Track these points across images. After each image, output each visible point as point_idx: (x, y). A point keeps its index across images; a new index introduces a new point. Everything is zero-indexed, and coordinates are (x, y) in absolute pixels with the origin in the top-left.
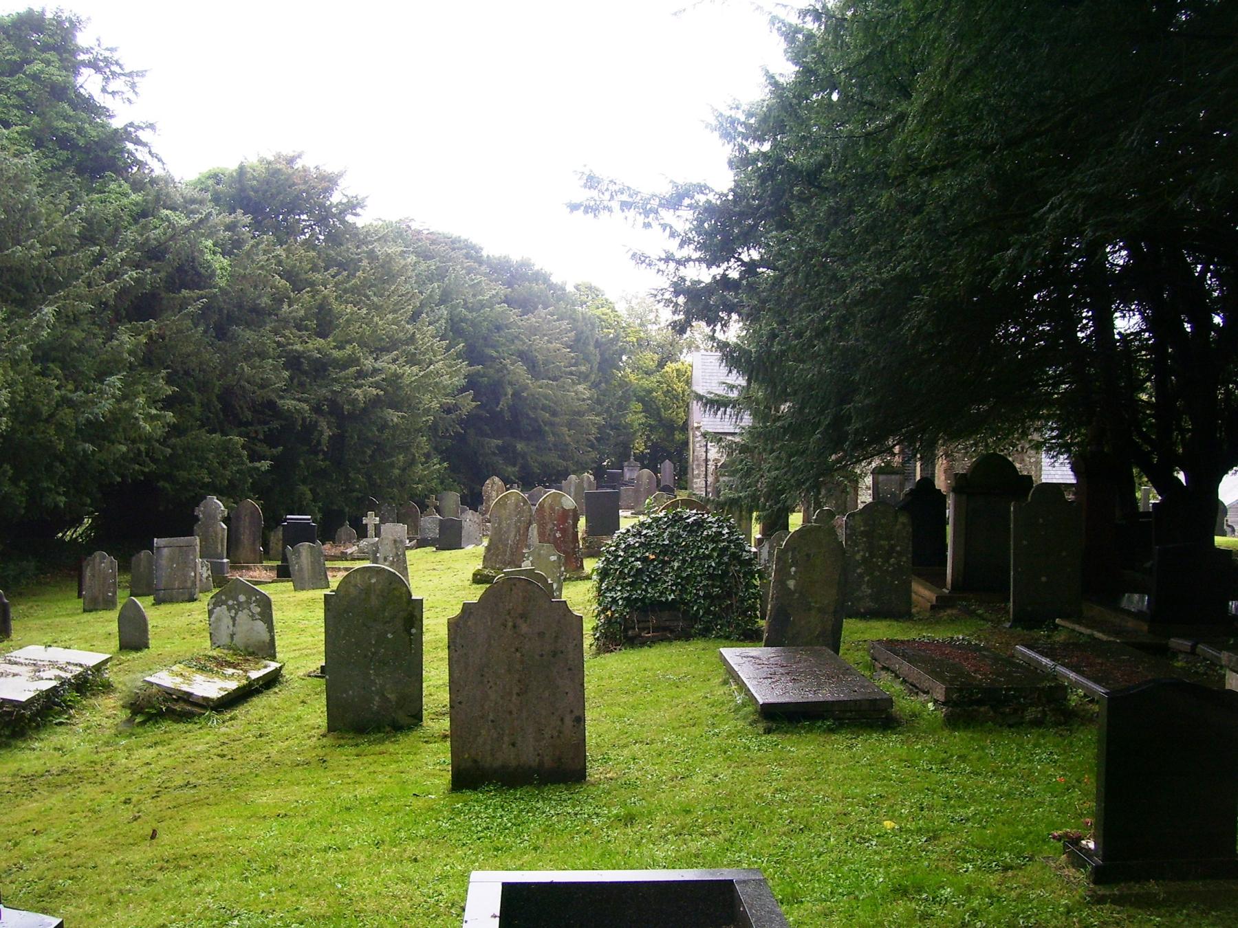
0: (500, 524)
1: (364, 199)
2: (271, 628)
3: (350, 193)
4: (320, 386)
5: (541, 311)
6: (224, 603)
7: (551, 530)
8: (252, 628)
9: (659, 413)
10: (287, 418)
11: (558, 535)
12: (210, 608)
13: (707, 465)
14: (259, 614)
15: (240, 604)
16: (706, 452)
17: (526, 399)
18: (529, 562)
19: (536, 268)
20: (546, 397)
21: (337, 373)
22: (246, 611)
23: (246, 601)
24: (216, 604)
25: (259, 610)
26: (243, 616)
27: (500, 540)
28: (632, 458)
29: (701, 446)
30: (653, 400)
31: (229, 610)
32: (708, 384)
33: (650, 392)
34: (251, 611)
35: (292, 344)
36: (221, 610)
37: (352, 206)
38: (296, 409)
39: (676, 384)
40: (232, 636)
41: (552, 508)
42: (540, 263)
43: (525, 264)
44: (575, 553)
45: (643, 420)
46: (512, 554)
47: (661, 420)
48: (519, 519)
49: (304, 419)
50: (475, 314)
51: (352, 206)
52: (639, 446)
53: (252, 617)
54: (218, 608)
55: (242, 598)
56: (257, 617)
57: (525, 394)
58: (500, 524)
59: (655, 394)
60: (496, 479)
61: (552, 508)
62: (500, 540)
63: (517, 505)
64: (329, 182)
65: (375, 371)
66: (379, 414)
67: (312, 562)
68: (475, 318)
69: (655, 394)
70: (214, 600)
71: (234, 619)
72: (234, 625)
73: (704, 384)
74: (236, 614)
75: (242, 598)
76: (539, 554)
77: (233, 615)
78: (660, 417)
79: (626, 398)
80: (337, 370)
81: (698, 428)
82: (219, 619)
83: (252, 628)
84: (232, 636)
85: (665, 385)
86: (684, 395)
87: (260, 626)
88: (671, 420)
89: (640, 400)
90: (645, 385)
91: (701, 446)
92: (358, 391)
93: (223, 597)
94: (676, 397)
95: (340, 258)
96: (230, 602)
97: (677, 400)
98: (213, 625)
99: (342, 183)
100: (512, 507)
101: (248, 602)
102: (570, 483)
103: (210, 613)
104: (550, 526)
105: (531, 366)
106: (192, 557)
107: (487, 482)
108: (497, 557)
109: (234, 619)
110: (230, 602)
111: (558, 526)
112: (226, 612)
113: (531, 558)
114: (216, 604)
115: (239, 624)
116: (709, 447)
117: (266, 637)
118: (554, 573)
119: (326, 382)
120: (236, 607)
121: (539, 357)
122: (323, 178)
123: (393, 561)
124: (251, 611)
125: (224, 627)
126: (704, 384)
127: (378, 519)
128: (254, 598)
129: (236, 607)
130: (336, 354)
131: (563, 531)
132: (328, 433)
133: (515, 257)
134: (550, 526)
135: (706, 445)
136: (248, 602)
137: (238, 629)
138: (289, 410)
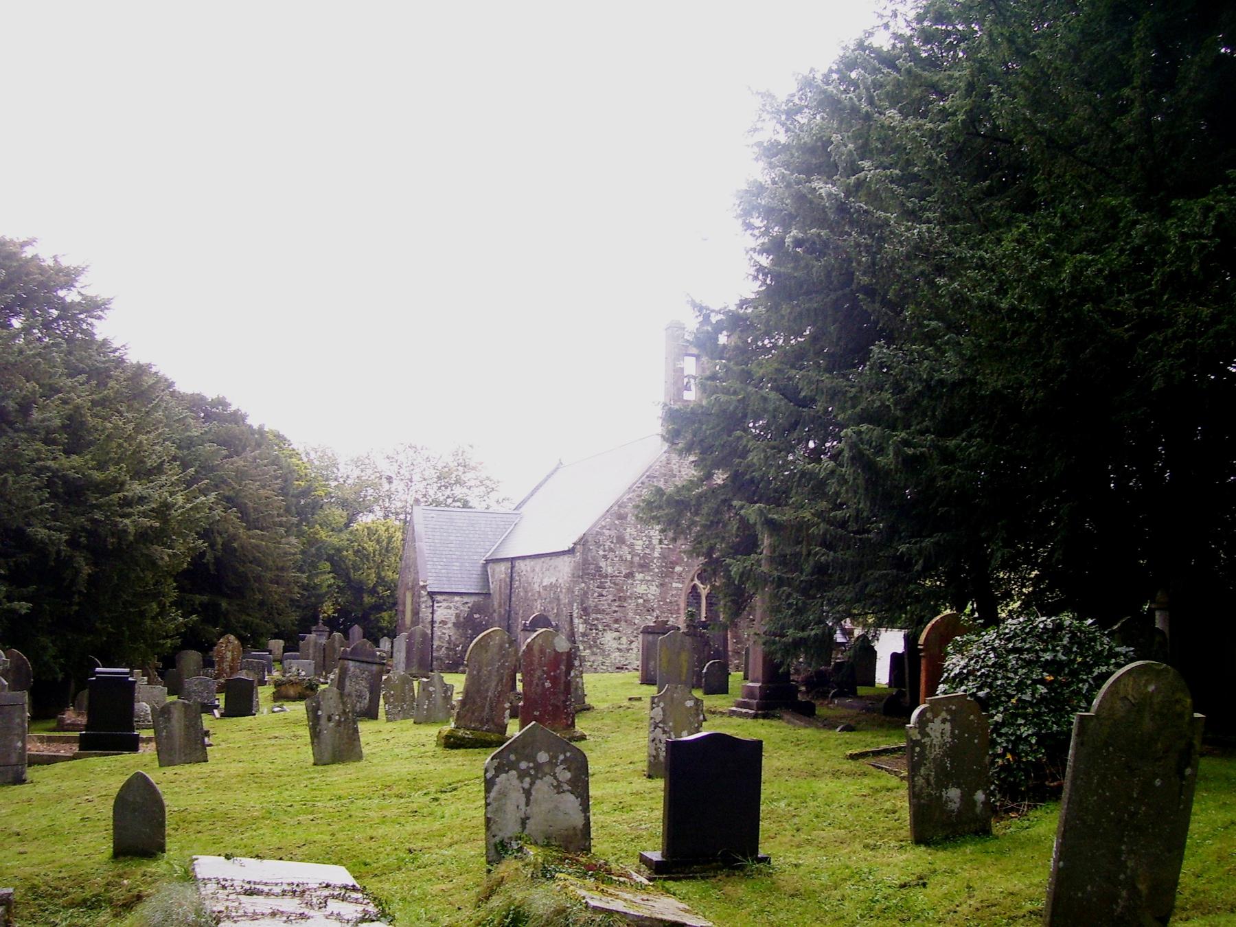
0: (479, 671)
1: (109, 301)
2: (585, 808)
3: (89, 292)
4: (75, 514)
5: (249, 454)
6: (513, 766)
7: (539, 679)
8: (556, 807)
9: (347, 574)
10: (39, 550)
11: (548, 684)
12: (489, 775)
13: (433, 627)
14: (569, 782)
15: (538, 767)
16: (433, 613)
17: (235, 550)
18: (659, 709)
19: (233, 408)
20: (257, 547)
21: (97, 499)
22: (548, 779)
23: (550, 762)
24: (499, 770)
25: (568, 775)
26: (543, 788)
27: (478, 691)
28: (321, 621)
29: (426, 607)
30: (342, 559)
31: (521, 777)
32: (430, 541)
33: (339, 550)
34: (555, 778)
35: (43, 460)
36: (508, 780)
37: (94, 307)
38: (50, 540)
39: (366, 543)
40: (524, 822)
41: (542, 651)
42: (236, 403)
43: (221, 402)
44: (566, 707)
45: (332, 581)
46: (492, 709)
47: (349, 580)
48: (503, 664)
49: (58, 552)
50: (186, 452)
51: (94, 307)
52: (328, 609)
53: (558, 788)
54: (504, 776)
55: (543, 757)
56: (566, 787)
57: (235, 545)
58: (479, 671)
59: (345, 553)
60: (232, 637)
61: (542, 651)
62: (478, 691)
63: (501, 647)
64: (68, 277)
65: (142, 500)
66: (145, 551)
67: (185, 725)
68: (185, 456)
69: (345, 553)
70: (496, 762)
71: (528, 793)
72: (527, 804)
73: (427, 540)
74: (532, 783)
75: (543, 757)
76: (672, 699)
77: (526, 786)
78: (349, 578)
79: (318, 556)
80: (97, 495)
81: (424, 587)
82: (503, 794)
83: (556, 807)
84: (524, 822)
85: (356, 544)
86: (374, 556)
87: (570, 802)
88: (360, 581)
89: (330, 559)
90: (334, 543)
91: (426, 607)
92: (127, 521)
93: (513, 757)
94: (367, 557)
95: (81, 365)
96: (523, 765)
97: (368, 560)
98: (495, 805)
99: (82, 280)
100: (495, 650)
101: (552, 763)
102: (308, 643)
103: (489, 784)
104: (538, 673)
105: (244, 515)
106: (18, 720)
107: (221, 640)
108: (473, 713)
109: (528, 793)
110: (523, 765)
111: (547, 673)
112: (516, 782)
113: (662, 705)
114: (499, 770)
115: (536, 800)
116: (435, 608)
117: (579, 821)
118: (691, 723)
119: (82, 508)
120: (532, 772)
121: (250, 504)
122: (59, 270)
123: (339, 721)
124: (555, 778)
125: (510, 807)
126: (427, 540)
127: (146, 678)
128: (562, 757)
129: (532, 772)
130: (97, 476)
131: (555, 680)
132: (87, 570)
133: (210, 395)
134: (538, 673)
135: (433, 606)
136: (552, 763)
137: (534, 810)
138: (42, 541)
